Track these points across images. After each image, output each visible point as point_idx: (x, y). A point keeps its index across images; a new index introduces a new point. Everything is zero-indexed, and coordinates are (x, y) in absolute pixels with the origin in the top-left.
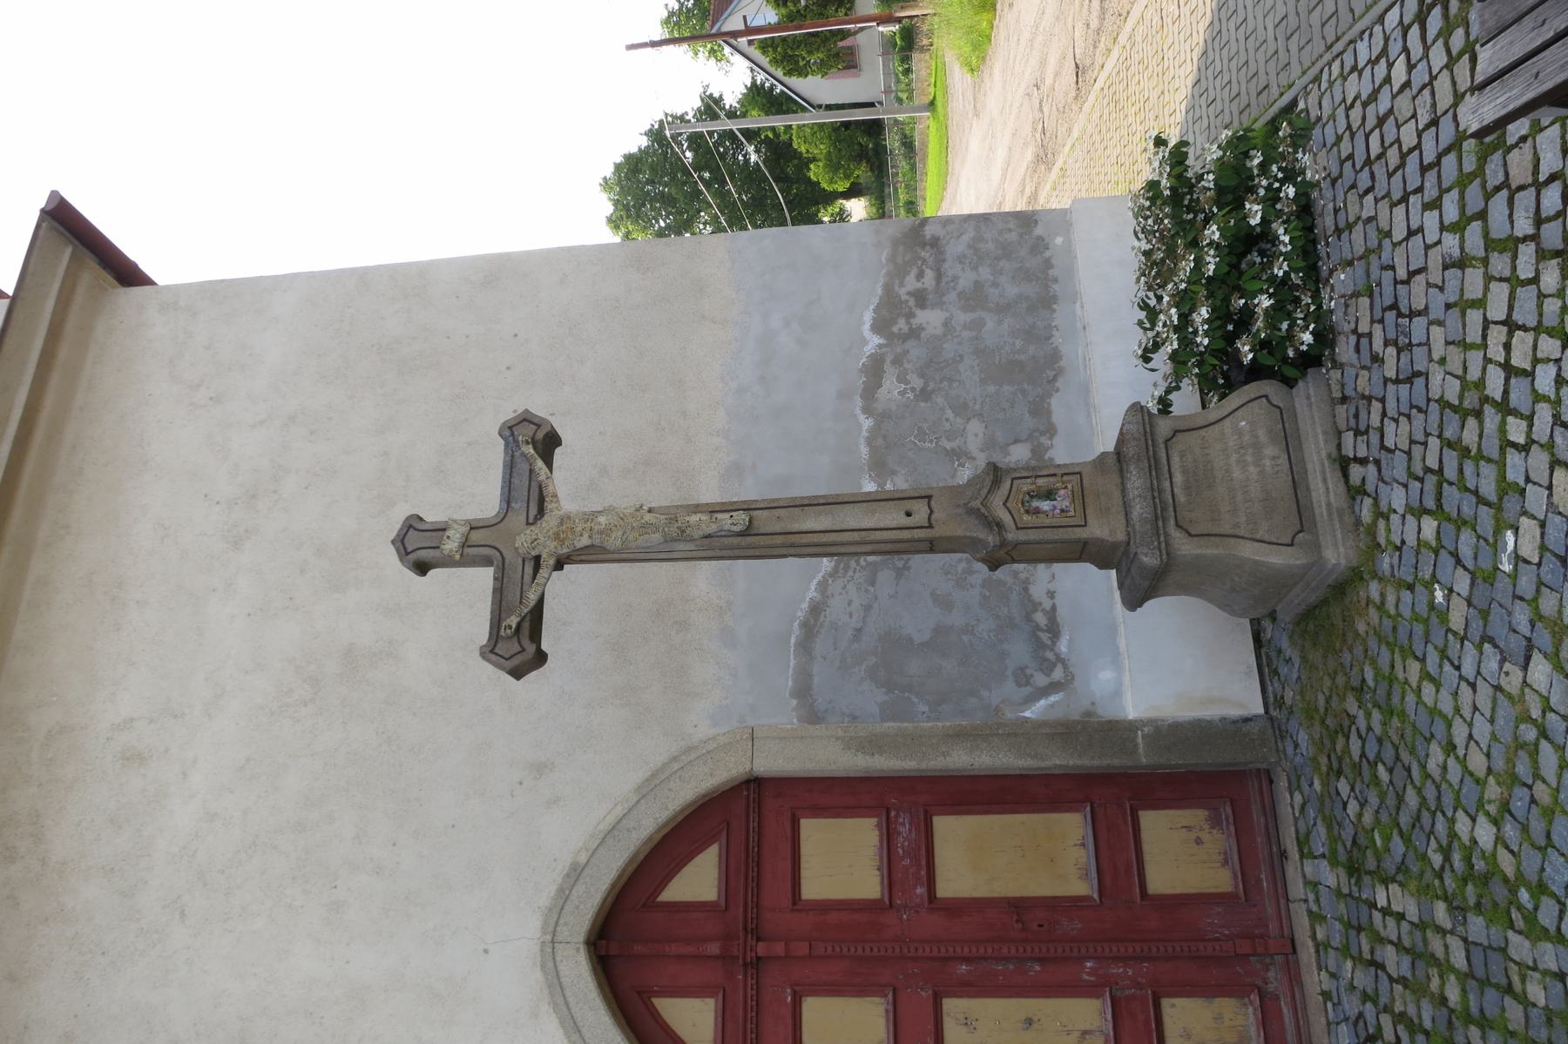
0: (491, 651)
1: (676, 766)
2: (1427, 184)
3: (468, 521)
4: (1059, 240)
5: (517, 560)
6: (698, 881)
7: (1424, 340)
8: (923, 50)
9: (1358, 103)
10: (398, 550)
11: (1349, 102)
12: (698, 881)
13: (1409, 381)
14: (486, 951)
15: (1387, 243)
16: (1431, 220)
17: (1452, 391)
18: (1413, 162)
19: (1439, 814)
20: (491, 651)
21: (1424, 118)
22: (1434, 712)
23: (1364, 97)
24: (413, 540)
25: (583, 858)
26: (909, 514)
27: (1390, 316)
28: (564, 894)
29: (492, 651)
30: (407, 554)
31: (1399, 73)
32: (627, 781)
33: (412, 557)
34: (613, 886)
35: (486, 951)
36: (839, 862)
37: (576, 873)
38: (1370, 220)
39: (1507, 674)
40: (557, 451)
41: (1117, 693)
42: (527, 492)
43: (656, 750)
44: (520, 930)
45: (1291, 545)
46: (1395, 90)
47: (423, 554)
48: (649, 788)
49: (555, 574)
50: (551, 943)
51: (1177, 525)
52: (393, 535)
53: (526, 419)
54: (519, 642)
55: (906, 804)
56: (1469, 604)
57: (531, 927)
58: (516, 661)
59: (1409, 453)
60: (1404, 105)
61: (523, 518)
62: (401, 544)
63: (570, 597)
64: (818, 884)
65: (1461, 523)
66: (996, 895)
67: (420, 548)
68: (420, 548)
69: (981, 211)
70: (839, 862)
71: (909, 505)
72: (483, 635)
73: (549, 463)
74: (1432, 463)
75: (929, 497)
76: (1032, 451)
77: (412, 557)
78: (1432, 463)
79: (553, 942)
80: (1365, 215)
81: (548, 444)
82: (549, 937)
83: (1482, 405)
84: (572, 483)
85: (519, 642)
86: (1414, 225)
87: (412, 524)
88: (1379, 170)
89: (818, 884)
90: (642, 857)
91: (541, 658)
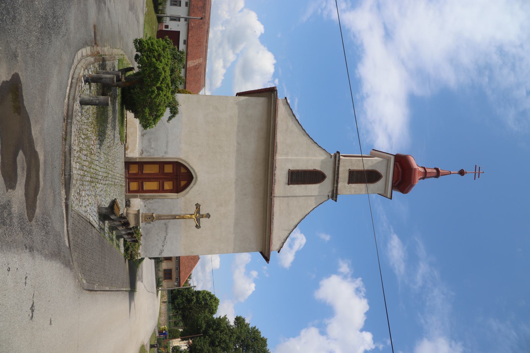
5: (199, 215)
6: (183, 183)
8: (172, 309)
28: (196, 182)
36: (168, 185)
37: (194, 184)
42: (198, 220)
43: (187, 196)
44: (199, 178)
48: (188, 192)
50: (196, 178)
54: (198, 206)
55: (161, 190)
57: (199, 178)
62: (210, 216)
63: (193, 210)
64: (171, 183)
66: (303, 186)
67: (208, 216)
68: (208, 216)
70: (168, 185)
72: (201, 207)
76: (94, 82)
81: (197, 226)
84: (193, 223)
87: (209, 218)
89: (171, 183)
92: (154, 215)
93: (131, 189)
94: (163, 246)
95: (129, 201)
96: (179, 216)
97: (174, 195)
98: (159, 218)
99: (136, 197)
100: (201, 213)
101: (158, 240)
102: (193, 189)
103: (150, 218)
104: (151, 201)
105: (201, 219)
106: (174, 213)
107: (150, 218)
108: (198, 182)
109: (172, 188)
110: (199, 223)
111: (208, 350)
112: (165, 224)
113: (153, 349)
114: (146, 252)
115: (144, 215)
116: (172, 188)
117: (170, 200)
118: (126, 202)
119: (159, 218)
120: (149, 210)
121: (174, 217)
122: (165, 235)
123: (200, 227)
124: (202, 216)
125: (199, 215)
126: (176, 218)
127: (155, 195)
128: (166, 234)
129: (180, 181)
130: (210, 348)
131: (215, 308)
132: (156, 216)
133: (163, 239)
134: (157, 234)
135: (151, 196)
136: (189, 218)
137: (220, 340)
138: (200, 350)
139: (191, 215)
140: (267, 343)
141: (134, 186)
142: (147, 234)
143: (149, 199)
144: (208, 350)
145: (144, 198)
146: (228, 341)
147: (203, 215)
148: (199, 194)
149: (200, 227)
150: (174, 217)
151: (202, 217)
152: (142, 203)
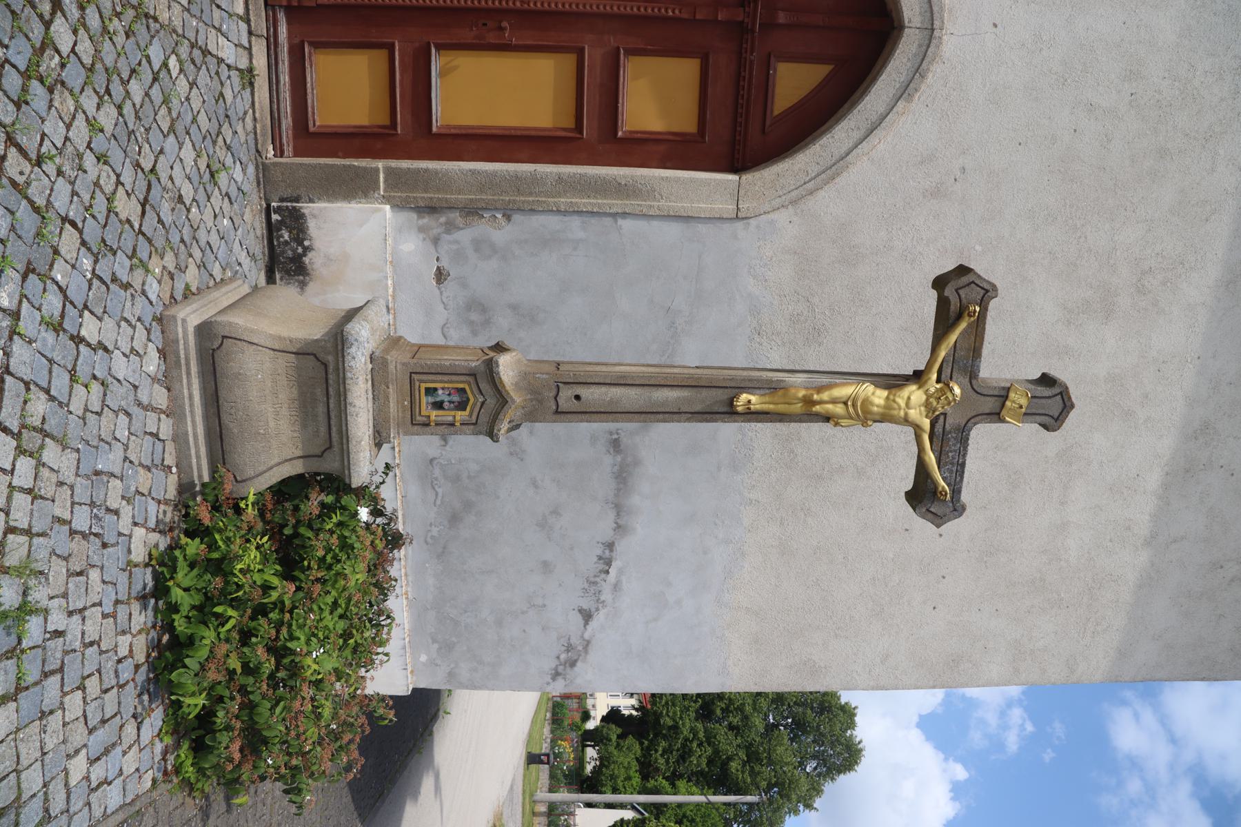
0: (987, 292)
1: (810, 185)
2: (59, 655)
3: (1003, 421)
4: (423, 658)
5: (964, 384)
6: (793, 82)
7: (77, 507)
9: (125, 746)
10: (1070, 398)
11: (135, 748)
12: (793, 82)
13: (97, 473)
14: (995, 26)
15: (108, 608)
16: (57, 620)
17: (51, 454)
18: (72, 677)
19: (81, 31)
20: (987, 292)
21: (55, 721)
22: (102, 158)
23: (119, 750)
24: (1055, 407)
25: (901, 104)
26: (578, 397)
27: (110, 538)
28: (918, 71)
29: (987, 291)
30: (1061, 393)
31: (78, 767)
32: (860, 171)
33: (1056, 390)
34: (875, 79)
35: (995, 26)
36: (655, 94)
37: (905, 91)
38: (124, 633)
39: (21, 173)
40: (909, 486)
41: (399, 230)
42: (948, 439)
43: (829, 203)
45: (224, 337)
46: (84, 751)
47: (1047, 392)
49: (922, 368)
50: (930, 31)
51: (326, 366)
52: (1072, 414)
53: (938, 520)
54: (960, 301)
55: (594, 133)
56: (56, 252)
57: (951, 44)
58: (965, 280)
59: (104, 404)
60: (78, 735)
61: (950, 421)
62: (1067, 405)
63: (904, 337)
64: (682, 73)
65: (58, 328)
67: (1051, 401)
68: (1051, 401)
69: (496, 692)
70: (655, 94)
71: (575, 405)
73: (922, 469)
74: (79, 390)
75: (557, 412)
77: (1056, 390)
78: (79, 390)
79: (933, 30)
80: (128, 637)
81: (922, 495)
82: (936, 33)
83: (20, 432)
84: (896, 457)
85: (960, 301)
86: (76, 618)
87: (1053, 422)
88: (110, 680)
89: (682, 73)
90: (846, 106)
91: (939, 283)
92: (507, 367)
93: (323, 116)
94: (587, 616)
95: (296, 222)
96: (772, 388)
97: (707, 188)
98: (563, 395)
99: (356, 187)
100: (991, 369)
101: (546, 567)
102: (882, 143)
103: (462, 394)
104: (501, 233)
105: (982, 437)
106: (695, 353)
107: (462, 394)
108: (936, 74)
109: (686, 123)
110: (957, 472)
111: (693, 731)
112: (615, 445)
113: (533, 767)
114: (447, 648)
115: (396, 360)
116: (686, 123)
117: (673, 230)
118: (271, 228)
119: (563, 395)
120: (476, 309)
121: (717, 399)
122: (605, 528)
123: (958, 509)
124: (994, 404)
125: (964, 384)
126: (729, 412)
127: (535, 179)
128: (619, 528)
129: (767, 66)
130: (699, 726)
131: (804, 786)
132: (528, 380)
133: (588, 562)
134: (543, 525)
135: (491, 182)
136: (864, 416)
137: (728, 707)
138: (670, 728)
139: (892, 382)
140: (857, 719)
141: (348, 85)
142: (454, 519)
143: (472, 211)
144: (693, 731)
145: (427, 206)
146: (748, 708)
147: (1003, 395)
148: (936, 193)
149: (958, 509)
150: (717, 399)
151: (996, 416)
152: (411, 246)
